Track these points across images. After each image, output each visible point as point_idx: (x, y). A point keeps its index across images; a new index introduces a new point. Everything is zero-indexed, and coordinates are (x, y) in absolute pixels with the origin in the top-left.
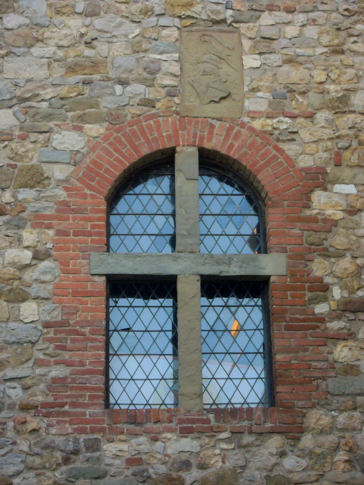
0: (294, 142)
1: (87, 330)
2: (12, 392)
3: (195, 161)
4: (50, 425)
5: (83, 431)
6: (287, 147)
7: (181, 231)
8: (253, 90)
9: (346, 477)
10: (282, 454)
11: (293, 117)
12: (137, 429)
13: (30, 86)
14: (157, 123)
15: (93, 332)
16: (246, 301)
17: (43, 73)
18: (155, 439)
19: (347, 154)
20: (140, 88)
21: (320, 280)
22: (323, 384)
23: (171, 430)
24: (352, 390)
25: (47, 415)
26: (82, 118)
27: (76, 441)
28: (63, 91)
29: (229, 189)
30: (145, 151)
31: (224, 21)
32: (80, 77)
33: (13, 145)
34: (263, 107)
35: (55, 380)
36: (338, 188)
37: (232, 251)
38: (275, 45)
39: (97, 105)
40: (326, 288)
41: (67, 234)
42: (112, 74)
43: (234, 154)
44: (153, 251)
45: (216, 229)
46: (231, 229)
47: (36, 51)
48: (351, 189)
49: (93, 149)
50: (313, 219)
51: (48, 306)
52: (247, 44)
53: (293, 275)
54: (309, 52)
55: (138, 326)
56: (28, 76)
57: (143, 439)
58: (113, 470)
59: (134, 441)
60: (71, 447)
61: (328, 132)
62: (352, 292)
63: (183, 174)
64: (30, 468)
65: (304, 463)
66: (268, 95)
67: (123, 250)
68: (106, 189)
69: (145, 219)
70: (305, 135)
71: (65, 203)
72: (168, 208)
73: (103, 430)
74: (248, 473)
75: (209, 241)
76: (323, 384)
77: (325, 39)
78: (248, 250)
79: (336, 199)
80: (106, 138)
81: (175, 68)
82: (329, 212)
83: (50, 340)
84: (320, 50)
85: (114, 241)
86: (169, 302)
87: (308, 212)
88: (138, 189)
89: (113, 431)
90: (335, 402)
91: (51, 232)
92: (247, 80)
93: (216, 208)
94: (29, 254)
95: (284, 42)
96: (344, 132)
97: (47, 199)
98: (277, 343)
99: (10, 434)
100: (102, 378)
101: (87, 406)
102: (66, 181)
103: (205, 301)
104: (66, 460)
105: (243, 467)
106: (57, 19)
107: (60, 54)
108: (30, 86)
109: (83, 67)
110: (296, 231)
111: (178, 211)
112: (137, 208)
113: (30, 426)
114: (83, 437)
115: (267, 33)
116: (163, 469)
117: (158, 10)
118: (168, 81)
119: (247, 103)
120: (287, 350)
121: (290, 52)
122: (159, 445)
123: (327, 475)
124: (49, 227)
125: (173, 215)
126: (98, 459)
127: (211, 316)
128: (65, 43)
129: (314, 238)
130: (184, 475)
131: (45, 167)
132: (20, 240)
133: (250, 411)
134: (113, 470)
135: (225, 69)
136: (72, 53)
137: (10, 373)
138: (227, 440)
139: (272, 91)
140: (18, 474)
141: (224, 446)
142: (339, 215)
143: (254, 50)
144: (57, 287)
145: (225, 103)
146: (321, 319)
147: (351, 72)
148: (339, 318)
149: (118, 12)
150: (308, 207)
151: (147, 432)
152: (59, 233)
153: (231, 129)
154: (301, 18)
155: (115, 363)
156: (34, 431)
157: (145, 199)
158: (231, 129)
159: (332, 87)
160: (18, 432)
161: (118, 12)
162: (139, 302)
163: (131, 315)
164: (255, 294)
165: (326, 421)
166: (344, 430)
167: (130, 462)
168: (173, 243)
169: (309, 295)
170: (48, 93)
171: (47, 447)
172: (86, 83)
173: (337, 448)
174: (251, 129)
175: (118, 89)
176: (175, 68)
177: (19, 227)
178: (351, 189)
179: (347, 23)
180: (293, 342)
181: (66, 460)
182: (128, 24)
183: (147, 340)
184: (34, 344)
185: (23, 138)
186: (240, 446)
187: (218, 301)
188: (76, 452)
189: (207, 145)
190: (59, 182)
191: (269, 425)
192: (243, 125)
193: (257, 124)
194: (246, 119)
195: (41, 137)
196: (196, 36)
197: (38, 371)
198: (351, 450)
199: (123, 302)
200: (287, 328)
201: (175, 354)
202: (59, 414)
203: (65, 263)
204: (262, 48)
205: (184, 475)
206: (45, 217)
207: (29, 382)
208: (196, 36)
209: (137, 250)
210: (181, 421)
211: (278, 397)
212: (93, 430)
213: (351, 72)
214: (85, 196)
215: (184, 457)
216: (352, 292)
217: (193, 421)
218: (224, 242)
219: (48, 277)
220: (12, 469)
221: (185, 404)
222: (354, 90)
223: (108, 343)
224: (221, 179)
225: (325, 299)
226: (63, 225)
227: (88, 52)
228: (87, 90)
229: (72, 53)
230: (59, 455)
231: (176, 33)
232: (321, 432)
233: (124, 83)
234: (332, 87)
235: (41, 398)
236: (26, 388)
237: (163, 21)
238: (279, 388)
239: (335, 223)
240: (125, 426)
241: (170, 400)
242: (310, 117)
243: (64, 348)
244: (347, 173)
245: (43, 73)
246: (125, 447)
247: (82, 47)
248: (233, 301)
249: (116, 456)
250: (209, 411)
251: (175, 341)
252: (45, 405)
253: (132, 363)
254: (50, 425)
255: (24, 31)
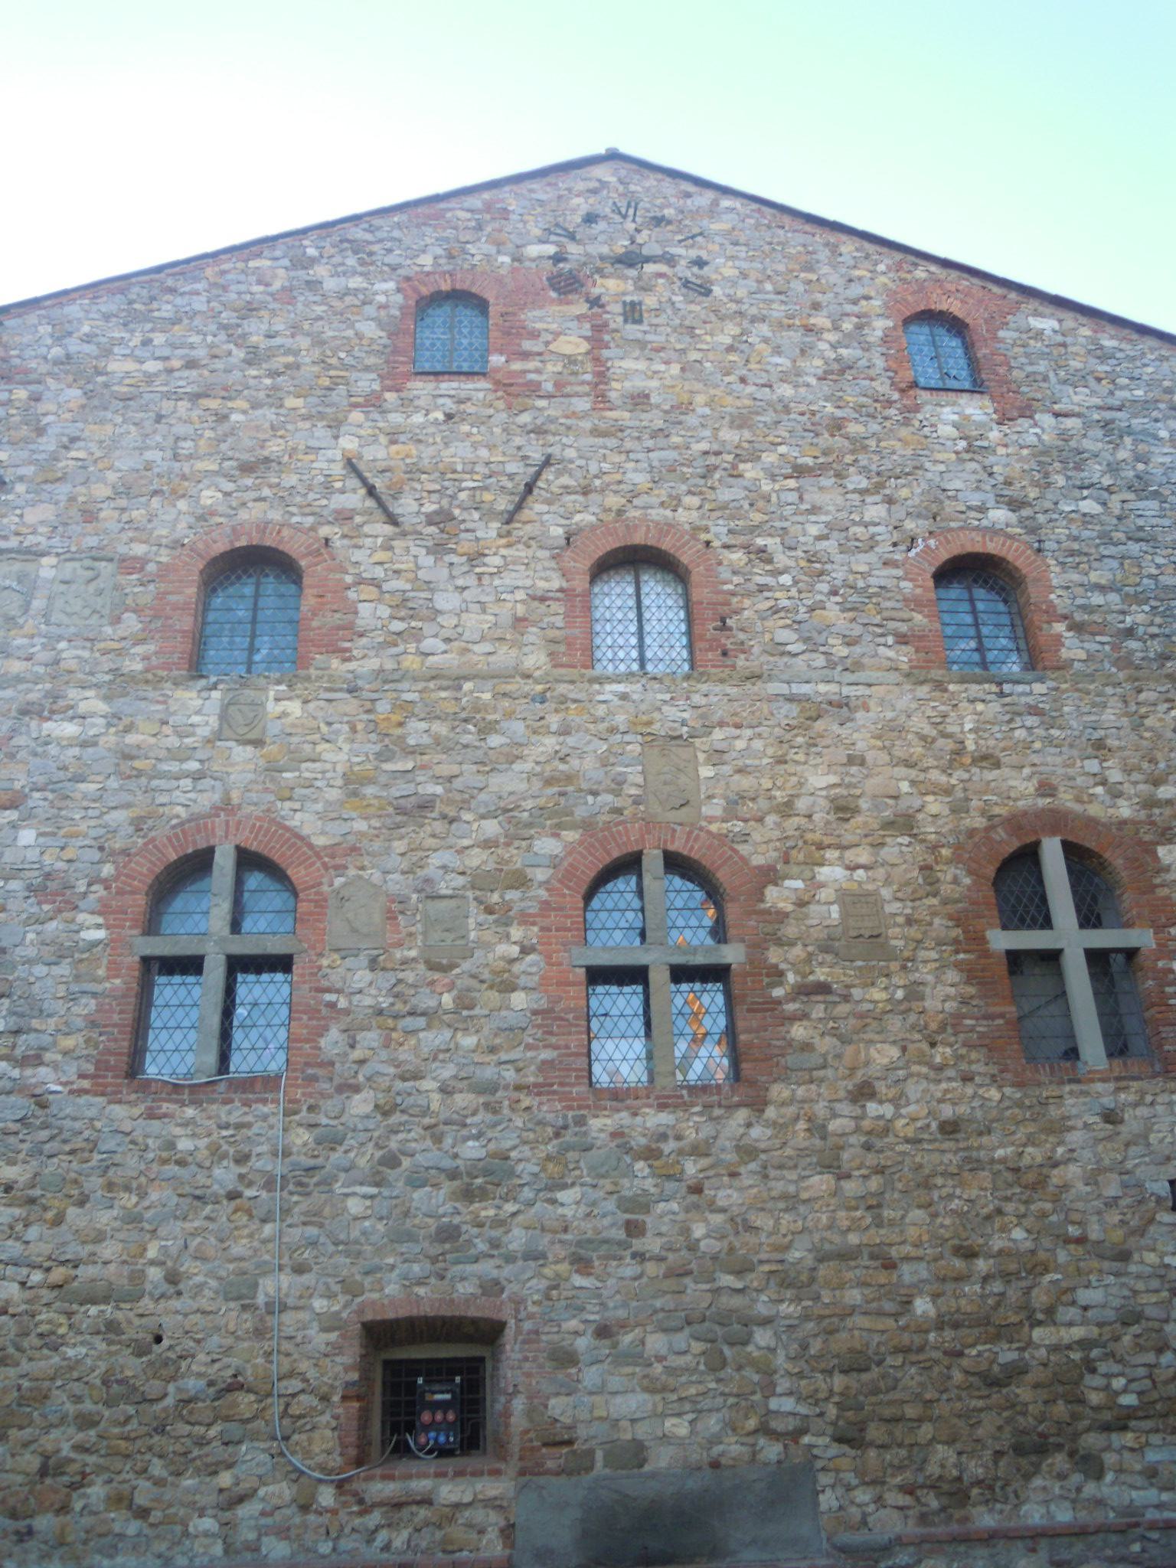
0: (679, 959)
1: (571, 1016)
2: (506, 1074)
3: (660, 862)
4: (541, 1104)
5: (570, 1108)
6: (740, 847)
7: (650, 925)
8: (710, 797)
9: (806, 1144)
10: (749, 1125)
11: (745, 821)
12: (619, 1105)
13: (512, 798)
14: (626, 828)
15: (576, 1018)
16: (709, 986)
17: (523, 786)
18: (635, 1114)
19: (794, 853)
20: (609, 798)
21: (776, 966)
22: (782, 1061)
23: (649, 1106)
24: (808, 1065)
25: (539, 1094)
26: (559, 826)
27: (565, 1117)
28: (541, 802)
29: (690, 886)
30: (616, 854)
31: (680, 737)
32: (556, 789)
33: (500, 851)
34: (718, 812)
35: (544, 1062)
36: (788, 883)
37: (695, 942)
38: (726, 757)
39: (572, 814)
40: (781, 974)
41: (549, 930)
42: (584, 786)
43: (693, 855)
44: (625, 943)
45: (680, 922)
46: (694, 922)
47: (518, 766)
48: (798, 884)
49: (570, 853)
50: (768, 912)
51: (535, 996)
52: (701, 757)
53: (751, 962)
54: (757, 762)
55: (614, 1012)
56: (510, 789)
57: (624, 1114)
58: (599, 1143)
59: (617, 1116)
60: (560, 1122)
61: (777, 834)
62: (804, 976)
63: (720, 999)
64: (525, 1143)
65: (769, 1132)
66: (722, 802)
67: (598, 944)
68: (584, 887)
69: (616, 915)
70: (756, 836)
71: (546, 902)
72: (636, 904)
73: (588, 1107)
74: (719, 1142)
75: (674, 933)
76: (782, 1061)
77: (770, 751)
78: (709, 941)
79: (786, 893)
80: (581, 843)
81: (640, 780)
82: (781, 905)
83: (539, 1026)
84: (766, 761)
85: (590, 935)
86: (640, 989)
87: (762, 906)
88: (609, 886)
89: (597, 1107)
90: (794, 1077)
91: (536, 929)
92: (703, 788)
93: (679, 903)
94: (516, 949)
95: (734, 754)
96: (790, 833)
97: (530, 899)
98: (740, 1024)
99: (506, 1111)
100: (585, 1059)
101: (572, 1085)
102: (547, 882)
103: (673, 987)
104: (557, 1135)
105: (715, 1138)
106: (534, 738)
107: (538, 769)
108: (512, 798)
109: (558, 780)
110: (752, 923)
111: (648, 907)
112: (609, 904)
113: (524, 1105)
114: (570, 1114)
115: (719, 746)
116: (643, 1141)
117: (622, 728)
118: (633, 791)
119: (703, 809)
120: (749, 1031)
121: (740, 763)
122: (639, 1119)
123: (791, 1143)
124: (534, 924)
125: (642, 910)
126: (585, 1134)
127: (679, 1001)
128: (542, 759)
129: (769, 929)
130: (662, 1146)
131: (528, 870)
132: (508, 936)
133: (718, 1086)
134: (599, 1143)
135: (683, 779)
136: (548, 768)
137: (504, 1057)
138: (700, 1114)
139: (726, 798)
140: (514, 1148)
141: (696, 1119)
142: (790, 908)
143: (709, 761)
144: (542, 978)
145: (684, 810)
146: (778, 1002)
147: (794, 779)
148: (794, 1000)
149: (587, 730)
150: (762, 901)
151: (628, 1108)
152: (542, 929)
153: (690, 833)
154: (748, 732)
155: (595, 1045)
156: (528, 1108)
157: (616, 896)
158: (690, 833)
159: (778, 793)
160: (513, 1110)
161: (587, 730)
162: (614, 989)
163: (608, 1002)
164: (716, 980)
165: (786, 1094)
166: (803, 1101)
167: (614, 1135)
168: (643, 935)
169: (766, 980)
170: (529, 804)
171: (540, 1123)
172: (562, 794)
173: (797, 1119)
174: (709, 832)
175: (590, 799)
176: (640, 780)
177: (507, 925)
178: (798, 884)
179: (788, 737)
180: (754, 1024)
181: (557, 1135)
182: (597, 742)
183: (622, 1024)
184: (524, 1029)
185: (508, 845)
186: (711, 1119)
187: (684, 987)
188: (565, 1127)
189: (671, 848)
190: (541, 884)
191: (736, 1099)
192: (701, 829)
193: (714, 828)
194: (704, 824)
195: (524, 844)
196: (656, 751)
197: (529, 1054)
198: (809, 1120)
199: (600, 989)
200: (749, 1010)
201: (648, 1034)
202: (549, 1093)
203: (548, 957)
204: (716, 758)
205: (662, 1146)
206: (530, 915)
207: (521, 1065)
208: (656, 751)
209: (611, 943)
210: (658, 1098)
211: (743, 1073)
212: (580, 1108)
213: (794, 779)
214: (564, 896)
215: (661, 1129)
216: (804, 976)
217: (669, 1097)
218: (688, 933)
219: (534, 969)
220: (509, 1144)
221: (660, 1082)
222: (798, 796)
223: (589, 1029)
224: (683, 876)
225: (781, 984)
226: (546, 922)
227: (562, 767)
228: (562, 800)
229: (548, 768)
230: (550, 1130)
231: (639, 749)
232: (783, 1104)
233: (595, 794)
234: (778, 793)
235: (532, 1079)
236: (518, 1070)
237: (627, 738)
238: (744, 1065)
239: (787, 915)
240: (609, 1104)
241: (644, 1078)
242: (760, 820)
243: (551, 1033)
244: (795, 870)
245: (523, 786)
246: (608, 1121)
247: (557, 763)
248: (697, 986)
249: (601, 1130)
250: (682, 1087)
251: (648, 1024)
252: (536, 1085)
253: (610, 1045)
254: (541, 1104)
255: (506, 749)
